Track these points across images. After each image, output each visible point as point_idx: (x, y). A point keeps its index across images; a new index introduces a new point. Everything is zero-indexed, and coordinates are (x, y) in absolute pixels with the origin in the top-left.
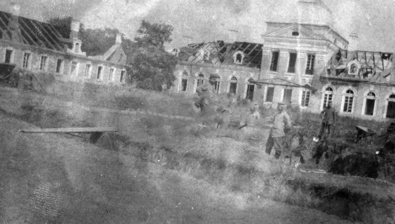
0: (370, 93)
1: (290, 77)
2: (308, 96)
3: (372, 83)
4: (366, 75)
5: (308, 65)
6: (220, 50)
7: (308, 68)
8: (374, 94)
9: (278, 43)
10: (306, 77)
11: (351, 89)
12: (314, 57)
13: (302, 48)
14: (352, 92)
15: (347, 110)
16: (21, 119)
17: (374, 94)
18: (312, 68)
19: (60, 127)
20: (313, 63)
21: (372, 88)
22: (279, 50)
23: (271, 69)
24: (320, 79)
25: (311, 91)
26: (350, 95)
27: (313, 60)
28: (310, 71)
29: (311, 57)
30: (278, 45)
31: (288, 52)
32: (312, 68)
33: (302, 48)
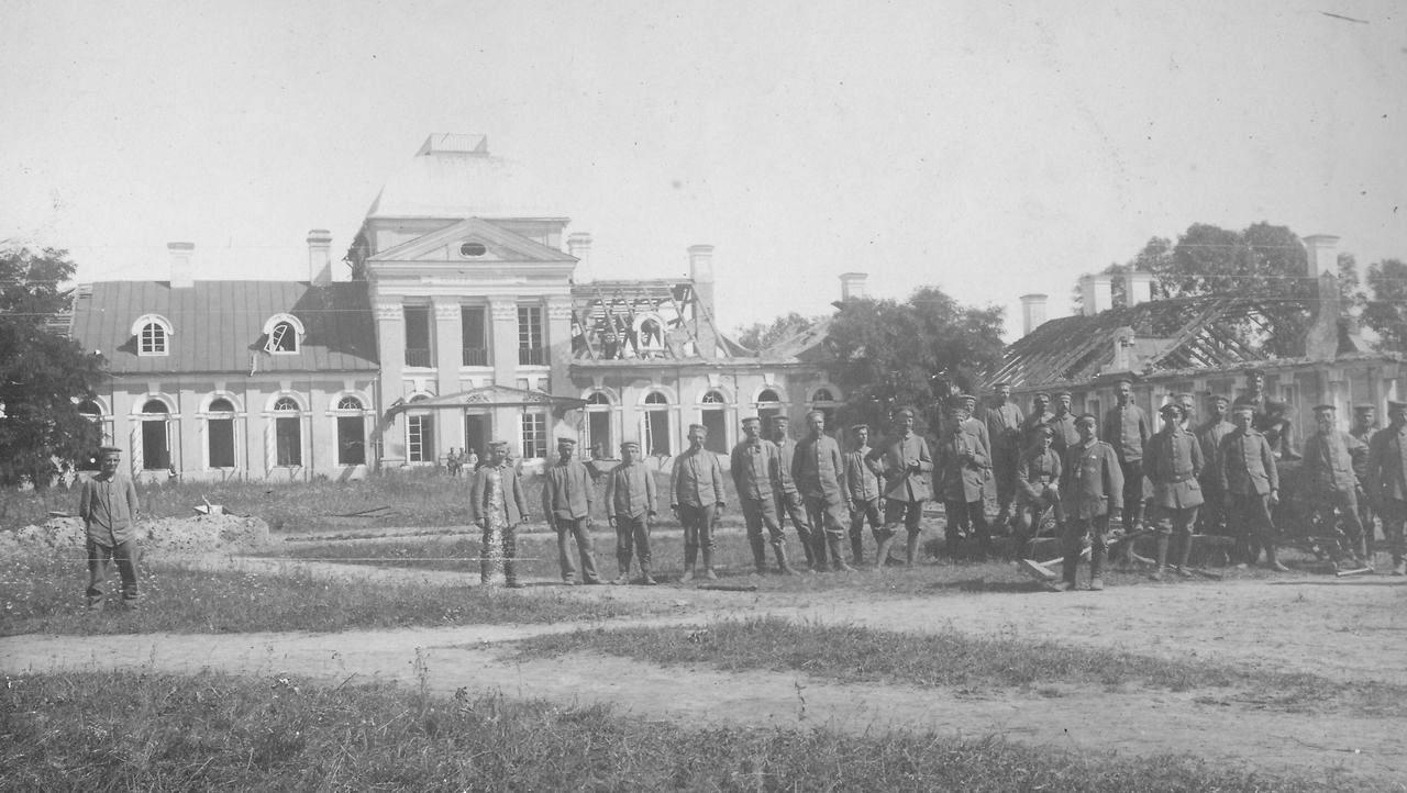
0: (709, 394)
1: (419, 381)
2: (541, 427)
3: (714, 368)
4: (610, 349)
5: (523, 337)
6: (735, 341)
7: (523, 346)
8: (719, 397)
9: (424, 281)
10: (528, 372)
11: (660, 391)
12: (536, 311)
13: (503, 291)
14: (662, 399)
15: (535, 455)
16: (1328, 433)
17: (719, 397)
18: (537, 344)
19: (278, 581)
20: (536, 329)
21: (715, 381)
22: (432, 303)
23: (407, 363)
24: (570, 376)
25: (548, 412)
26: (658, 407)
27: (536, 319)
28: (533, 353)
29: (531, 317)
30: (425, 285)
31: (514, 306)
32: (537, 344)
33: (503, 291)
